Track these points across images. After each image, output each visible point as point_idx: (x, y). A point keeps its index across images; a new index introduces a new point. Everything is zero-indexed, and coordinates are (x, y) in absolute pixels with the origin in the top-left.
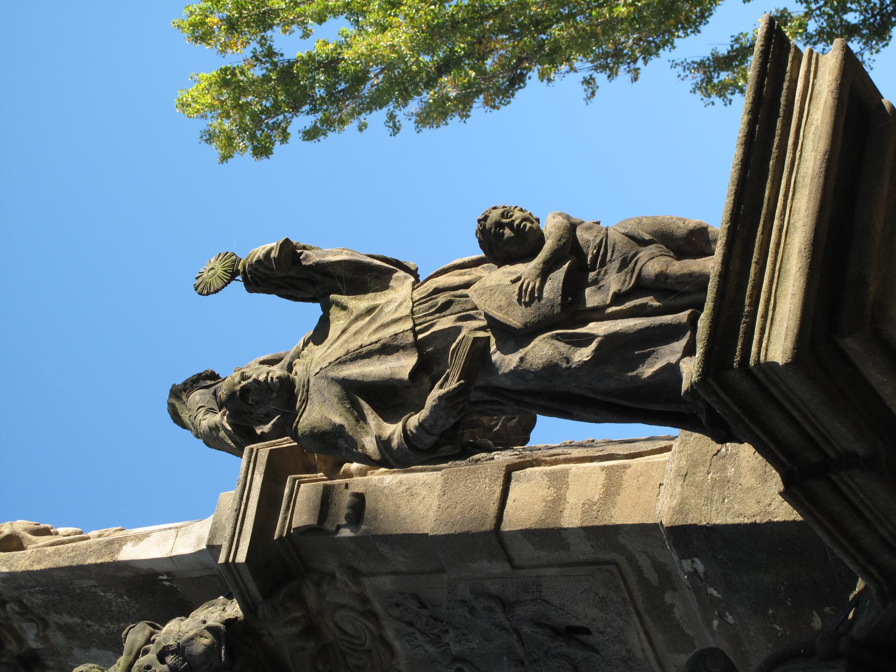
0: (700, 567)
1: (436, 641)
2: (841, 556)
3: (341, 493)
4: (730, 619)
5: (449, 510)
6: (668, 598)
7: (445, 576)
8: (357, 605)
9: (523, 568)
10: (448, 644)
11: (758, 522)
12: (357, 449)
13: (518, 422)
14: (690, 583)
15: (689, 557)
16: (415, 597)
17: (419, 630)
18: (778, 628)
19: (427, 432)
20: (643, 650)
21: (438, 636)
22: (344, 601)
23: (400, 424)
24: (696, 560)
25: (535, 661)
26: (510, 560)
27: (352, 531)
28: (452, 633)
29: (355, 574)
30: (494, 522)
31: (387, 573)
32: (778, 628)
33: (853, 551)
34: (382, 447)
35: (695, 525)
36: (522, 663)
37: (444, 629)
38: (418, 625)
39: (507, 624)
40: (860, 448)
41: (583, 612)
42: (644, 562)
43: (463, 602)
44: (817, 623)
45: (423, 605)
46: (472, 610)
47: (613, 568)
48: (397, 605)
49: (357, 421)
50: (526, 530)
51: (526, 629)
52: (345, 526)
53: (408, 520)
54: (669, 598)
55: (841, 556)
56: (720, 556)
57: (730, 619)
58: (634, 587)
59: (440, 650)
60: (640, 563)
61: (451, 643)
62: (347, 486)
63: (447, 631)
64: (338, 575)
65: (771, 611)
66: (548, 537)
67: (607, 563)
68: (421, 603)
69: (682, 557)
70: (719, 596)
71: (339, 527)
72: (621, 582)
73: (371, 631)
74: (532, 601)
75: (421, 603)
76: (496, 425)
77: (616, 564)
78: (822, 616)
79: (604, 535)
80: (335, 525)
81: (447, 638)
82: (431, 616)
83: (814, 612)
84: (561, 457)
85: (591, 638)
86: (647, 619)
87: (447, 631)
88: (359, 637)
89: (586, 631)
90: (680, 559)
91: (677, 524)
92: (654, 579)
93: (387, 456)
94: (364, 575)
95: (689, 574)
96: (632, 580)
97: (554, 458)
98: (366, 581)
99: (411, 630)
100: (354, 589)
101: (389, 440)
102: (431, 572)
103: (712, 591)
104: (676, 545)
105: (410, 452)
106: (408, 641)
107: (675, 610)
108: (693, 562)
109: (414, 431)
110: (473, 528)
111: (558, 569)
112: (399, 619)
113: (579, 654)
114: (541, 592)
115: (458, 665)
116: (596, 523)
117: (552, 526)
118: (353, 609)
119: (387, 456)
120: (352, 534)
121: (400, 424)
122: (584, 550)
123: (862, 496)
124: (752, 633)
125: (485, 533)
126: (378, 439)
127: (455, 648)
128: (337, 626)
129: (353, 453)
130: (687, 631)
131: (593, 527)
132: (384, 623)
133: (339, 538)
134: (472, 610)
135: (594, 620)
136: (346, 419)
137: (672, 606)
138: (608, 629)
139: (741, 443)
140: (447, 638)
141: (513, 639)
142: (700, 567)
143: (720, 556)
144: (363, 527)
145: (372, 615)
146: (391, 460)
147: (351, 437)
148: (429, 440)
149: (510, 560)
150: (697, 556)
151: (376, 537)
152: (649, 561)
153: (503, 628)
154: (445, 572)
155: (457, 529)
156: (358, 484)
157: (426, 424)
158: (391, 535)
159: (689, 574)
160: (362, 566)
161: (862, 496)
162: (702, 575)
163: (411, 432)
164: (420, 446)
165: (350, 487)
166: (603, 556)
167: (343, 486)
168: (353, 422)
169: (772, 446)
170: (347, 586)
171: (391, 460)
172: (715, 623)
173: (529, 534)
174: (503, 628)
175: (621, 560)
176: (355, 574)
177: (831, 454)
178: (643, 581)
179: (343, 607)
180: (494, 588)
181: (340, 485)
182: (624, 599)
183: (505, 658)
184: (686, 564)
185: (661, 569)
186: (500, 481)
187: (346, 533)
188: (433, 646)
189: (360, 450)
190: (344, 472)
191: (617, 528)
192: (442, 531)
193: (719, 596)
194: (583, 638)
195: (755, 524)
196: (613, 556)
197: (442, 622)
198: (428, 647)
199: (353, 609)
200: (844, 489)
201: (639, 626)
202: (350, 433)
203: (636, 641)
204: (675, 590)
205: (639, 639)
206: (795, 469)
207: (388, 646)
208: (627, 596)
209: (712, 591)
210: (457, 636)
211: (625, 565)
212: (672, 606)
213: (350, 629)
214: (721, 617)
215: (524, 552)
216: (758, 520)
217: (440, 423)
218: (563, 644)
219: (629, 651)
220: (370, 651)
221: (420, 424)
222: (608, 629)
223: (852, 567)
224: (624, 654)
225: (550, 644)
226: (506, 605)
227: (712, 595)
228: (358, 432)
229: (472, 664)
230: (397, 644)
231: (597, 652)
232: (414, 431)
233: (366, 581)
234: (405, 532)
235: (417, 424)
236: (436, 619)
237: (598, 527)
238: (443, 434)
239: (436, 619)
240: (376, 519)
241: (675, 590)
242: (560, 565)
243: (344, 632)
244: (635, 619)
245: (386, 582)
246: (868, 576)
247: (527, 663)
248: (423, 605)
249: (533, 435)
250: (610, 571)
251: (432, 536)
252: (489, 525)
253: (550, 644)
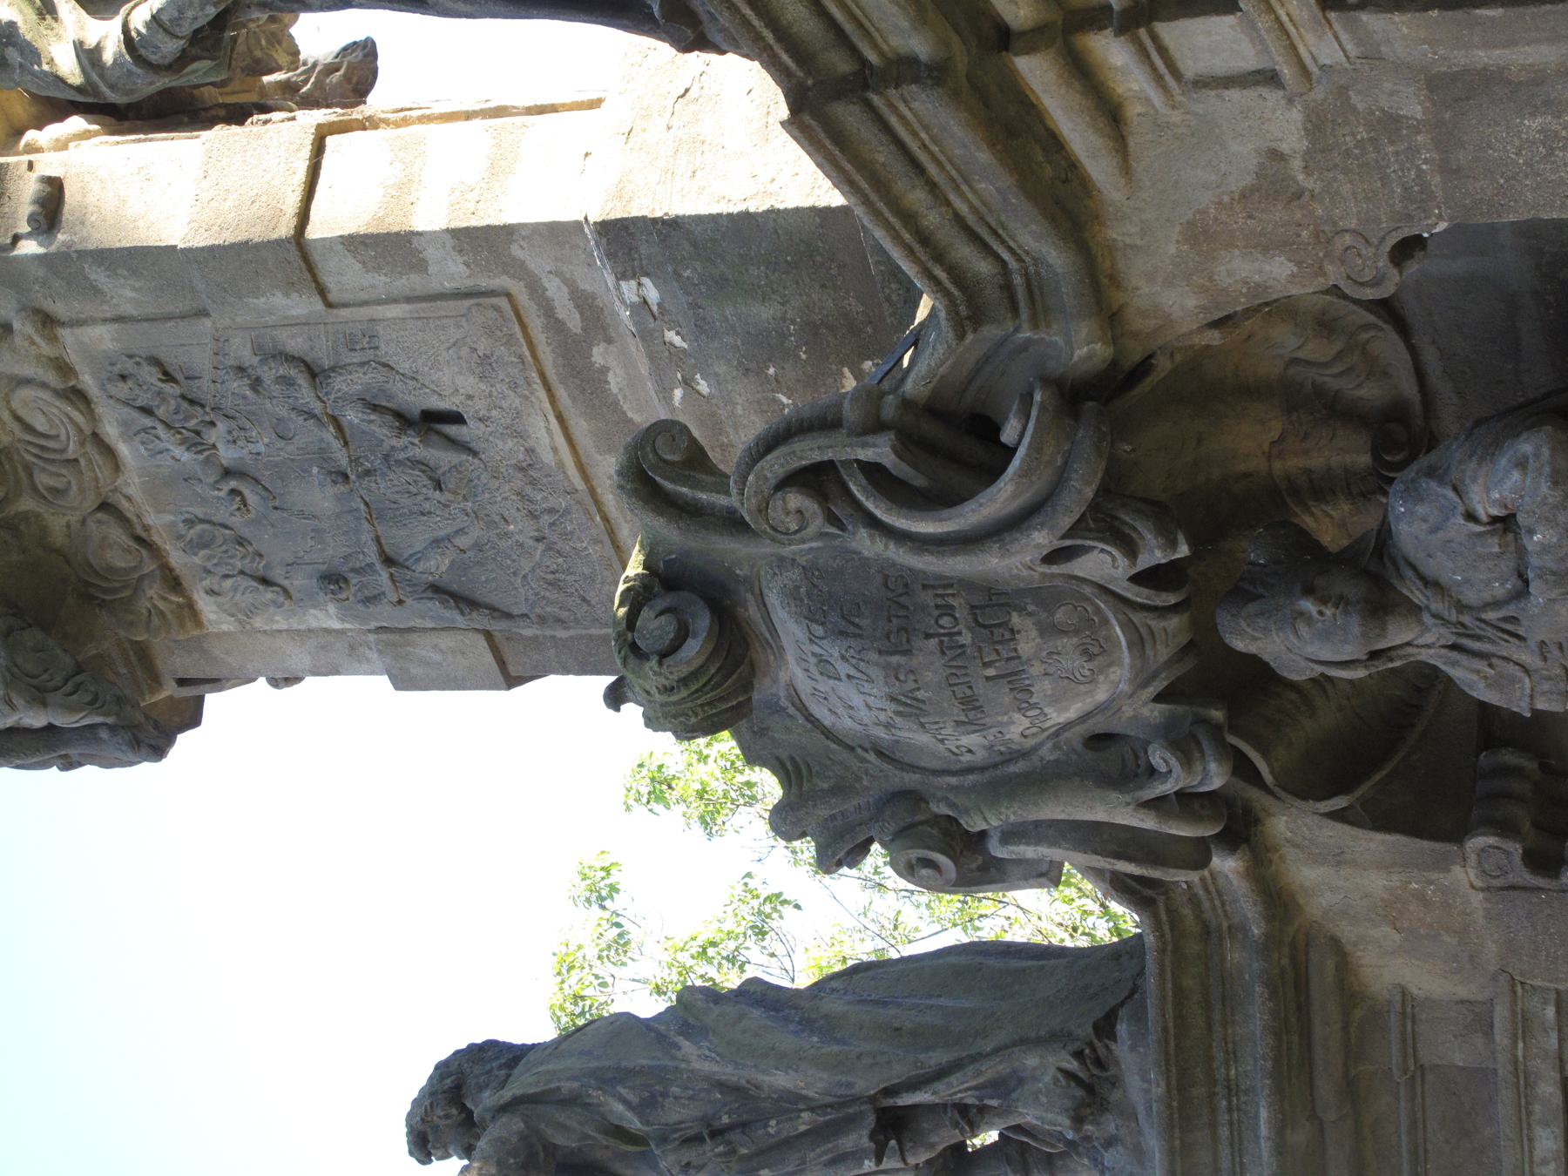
0: (652, 294)
1: (195, 441)
2: (887, 244)
3: (20, 177)
4: (703, 387)
5: (214, 204)
6: (599, 355)
7: (208, 323)
8: (52, 378)
9: (346, 305)
10: (214, 446)
11: (752, 210)
12: (40, 65)
13: (344, 75)
14: (635, 324)
15: (634, 277)
16: (155, 362)
17: (162, 421)
18: (785, 400)
19: (166, 31)
20: (555, 450)
21: (198, 433)
22: (28, 370)
23: (117, 22)
24: (646, 281)
25: (368, 473)
26: (322, 292)
27: (41, 244)
28: (222, 426)
29: (47, 322)
30: (294, 222)
31: (105, 320)
32: (785, 400)
33: (907, 236)
34: (86, 62)
35: (644, 218)
36: (346, 477)
37: (207, 419)
38: (160, 412)
39: (317, 407)
40: (920, 46)
41: (448, 383)
42: (555, 290)
43: (241, 370)
44: (850, 383)
45: (168, 377)
46: (256, 384)
47: (503, 303)
48: (123, 377)
49: (41, 15)
50: (351, 237)
51: (352, 416)
52: (29, 236)
53: (141, 223)
54: (599, 355)
55: (887, 244)
56: (687, 273)
57: (703, 387)
58: (540, 337)
59: (201, 457)
60: (549, 293)
61: (219, 446)
62: (31, 166)
63: (212, 424)
64: (16, 325)
65: (771, 371)
66: (389, 249)
67: (491, 293)
68: (165, 373)
69: (622, 276)
70: (685, 345)
71: (16, 239)
72: (517, 328)
73: (76, 425)
74: (362, 364)
75: (165, 373)
76: (306, 82)
77: (508, 295)
78: (858, 375)
79: (484, 243)
80: (10, 234)
81: (212, 436)
82: (183, 397)
83: (846, 370)
84: (415, 114)
85: (464, 429)
86: (561, 393)
87: (212, 424)
88: (56, 437)
89: (457, 418)
90: (618, 279)
91: (612, 216)
92: (574, 323)
93: (95, 78)
94: (63, 324)
95: (633, 307)
96: (536, 324)
97: (402, 114)
98: (65, 334)
99: (147, 422)
100: (46, 349)
101: (98, 50)
102: (183, 317)
103: (672, 336)
104: (611, 255)
105: (134, 69)
106: (143, 443)
107: (610, 377)
108: (639, 284)
109: (144, 31)
110: (257, 234)
111: (406, 307)
112: (126, 403)
113: (442, 458)
114: (377, 348)
115: (233, 484)
116: (475, 222)
117: (395, 229)
118: (44, 385)
119: (95, 78)
120: (41, 250)
121: (117, 22)
122: (451, 271)
123: (923, 135)
124: (739, 410)
125: (278, 243)
126: (79, 46)
127: (227, 455)
128: (18, 418)
129: (34, 74)
130: (630, 415)
131: (467, 229)
132: (100, 410)
133: (16, 258)
134: (256, 384)
135: (470, 397)
136: (21, 11)
137: (604, 370)
138: (494, 413)
139: (723, 52)
140: (212, 436)
141: (329, 435)
142: (652, 294)
143: (687, 273)
144: (61, 237)
145: (78, 396)
146: (101, 84)
147: (29, 44)
148: (170, 47)
149: (322, 292)
150: (647, 275)
151: (83, 254)
152: (565, 289)
153: (310, 415)
154: (207, 315)
155: (228, 237)
156: (49, 165)
157: (165, 17)
158: (110, 250)
159: (633, 307)
160: (59, 309)
161: (923, 135)
162: (655, 309)
163: (139, 33)
164: (153, 58)
165: (36, 166)
166: (484, 283)
167: (25, 166)
168: (33, 17)
169: (769, 36)
170: (33, 343)
171: (101, 84)
172: (678, 393)
173: (355, 244)
174: (310, 415)
175: (518, 289)
176: (47, 322)
177: (873, 57)
178: (555, 325)
179: (26, 382)
180: (296, 343)
181: (17, 164)
182: (521, 357)
183: (315, 470)
184: (629, 289)
185: (587, 304)
186: (306, 152)
187: (29, 247)
188: (188, 449)
189: (46, 67)
190: (27, 145)
191: (509, 231)
192: (201, 241)
193: (685, 345)
194: (451, 430)
195: (746, 215)
196: (502, 282)
197: (203, 406)
198: (179, 452)
199: (44, 385)
200: (893, 121)
201: (547, 405)
202: (28, 37)
203: (544, 434)
204: (609, 341)
205: (548, 430)
206: (810, 82)
207: (109, 451)
208: (527, 353)
209: (672, 336)
210: (230, 432)
211: (523, 298)
212: (604, 370)
213: (40, 424)
214: (688, 383)
215: (345, 277)
216: (753, 207)
217: (190, 14)
218: (416, 441)
219: (530, 451)
220: (76, 460)
221: (153, 17)
222: (494, 413)
223: (908, 267)
224: (521, 457)
225: (394, 442)
226: (314, 373)
227: (671, 344)
228: (41, 36)
229: (257, 481)
230: (123, 449)
231: (475, 454)
232: (144, 31)
233: (65, 334)
234: (135, 244)
235: (148, 17)
236: (192, 402)
237: (476, 229)
238: (196, 37)
239: (192, 402)
240: (83, 223)
241: (609, 341)
242: (409, 300)
243: (30, 429)
244: (542, 394)
245: (102, 337)
246: (937, 287)
247: (353, 477)
248: (168, 377)
249: (370, 98)
250: (497, 309)
251: (183, 250)
252: (285, 229)
253: (394, 442)
